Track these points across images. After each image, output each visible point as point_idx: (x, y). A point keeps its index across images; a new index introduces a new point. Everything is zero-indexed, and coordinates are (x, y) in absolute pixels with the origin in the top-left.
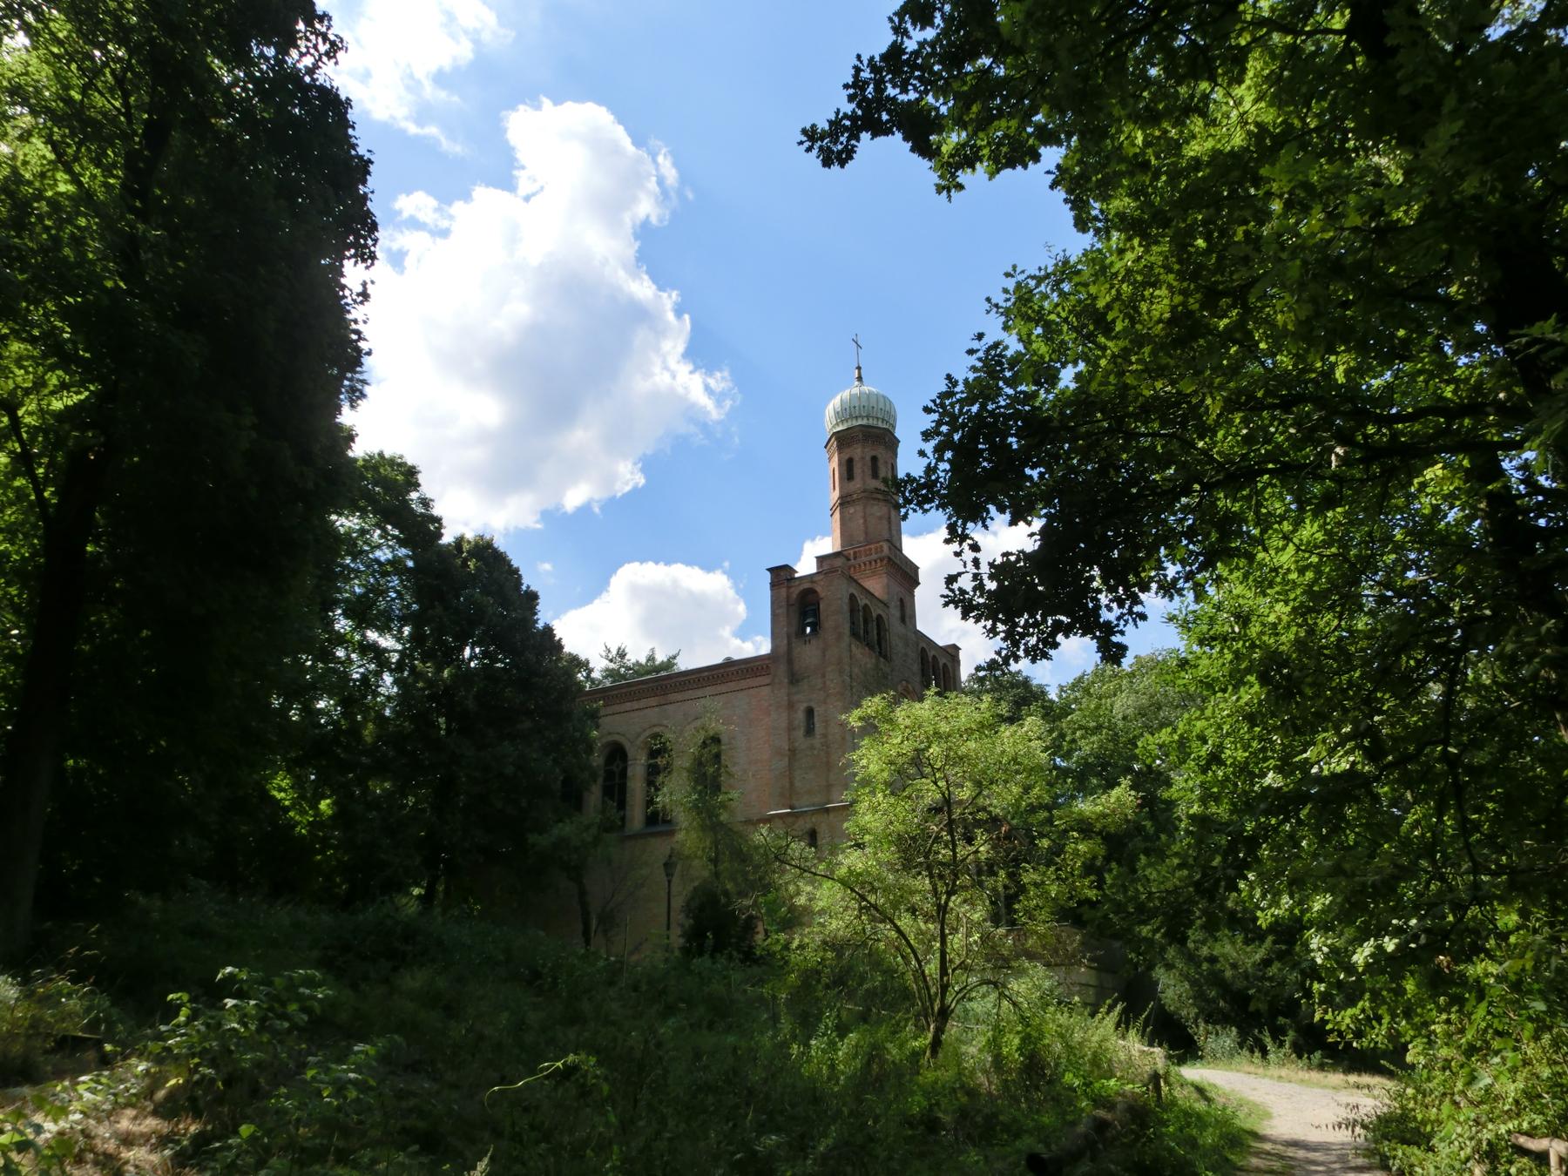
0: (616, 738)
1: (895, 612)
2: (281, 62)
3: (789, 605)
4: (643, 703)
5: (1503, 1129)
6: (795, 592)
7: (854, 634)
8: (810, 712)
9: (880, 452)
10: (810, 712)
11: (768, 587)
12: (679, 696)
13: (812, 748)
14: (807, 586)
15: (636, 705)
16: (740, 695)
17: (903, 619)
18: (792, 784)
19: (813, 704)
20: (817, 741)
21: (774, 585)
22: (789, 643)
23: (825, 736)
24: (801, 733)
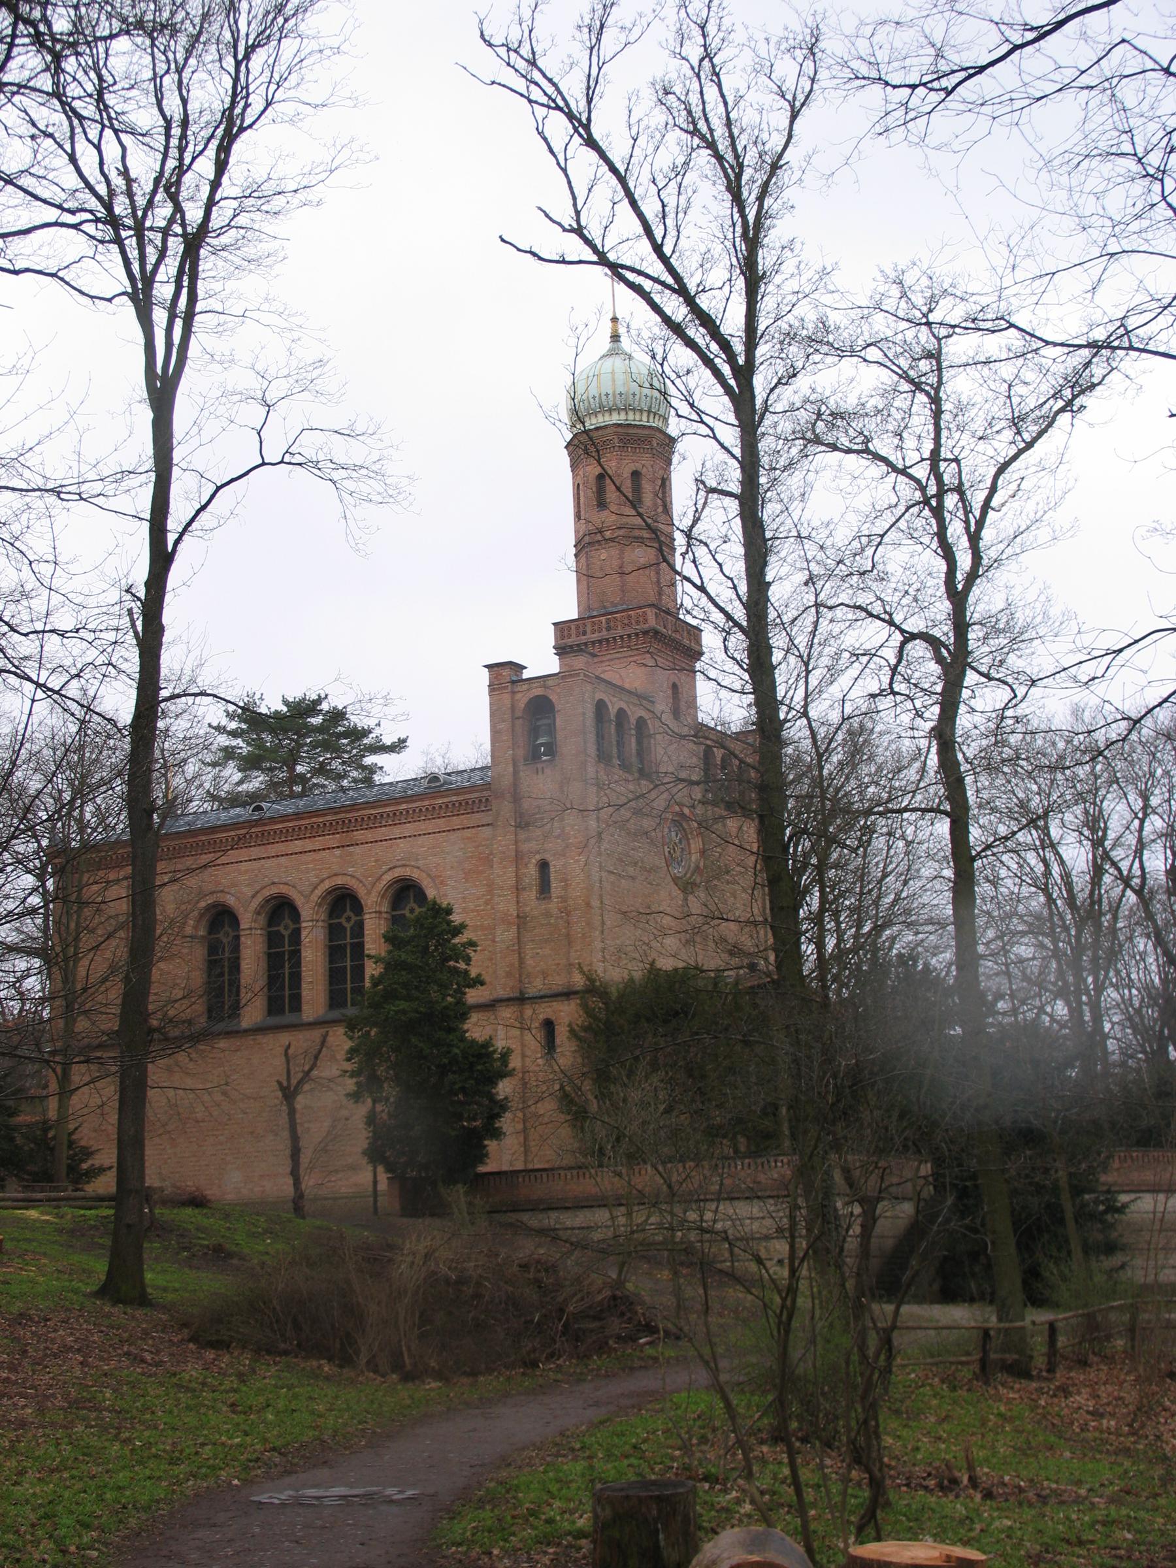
0: (284, 890)
1: (662, 706)
2: (620, 1283)
3: (514, 718)
4: (318, 843)
5: (108, 955)
6: (522, 700)
7: (603, 757)
8: (544, 866)
9: (645, 464)
10: (544, 866)
11: (486, 690)
12: (369, 835)
13: (547, 914)
14: (538, 692)
15: (308, 845)
16: (453, 836)
17: (676, 713)
18: (521, 961)
19: (548, 857)
20: (553, 906)
21: (494, 688)
22: (516, 773)
23: (564, 899)
24: (531, 895)
